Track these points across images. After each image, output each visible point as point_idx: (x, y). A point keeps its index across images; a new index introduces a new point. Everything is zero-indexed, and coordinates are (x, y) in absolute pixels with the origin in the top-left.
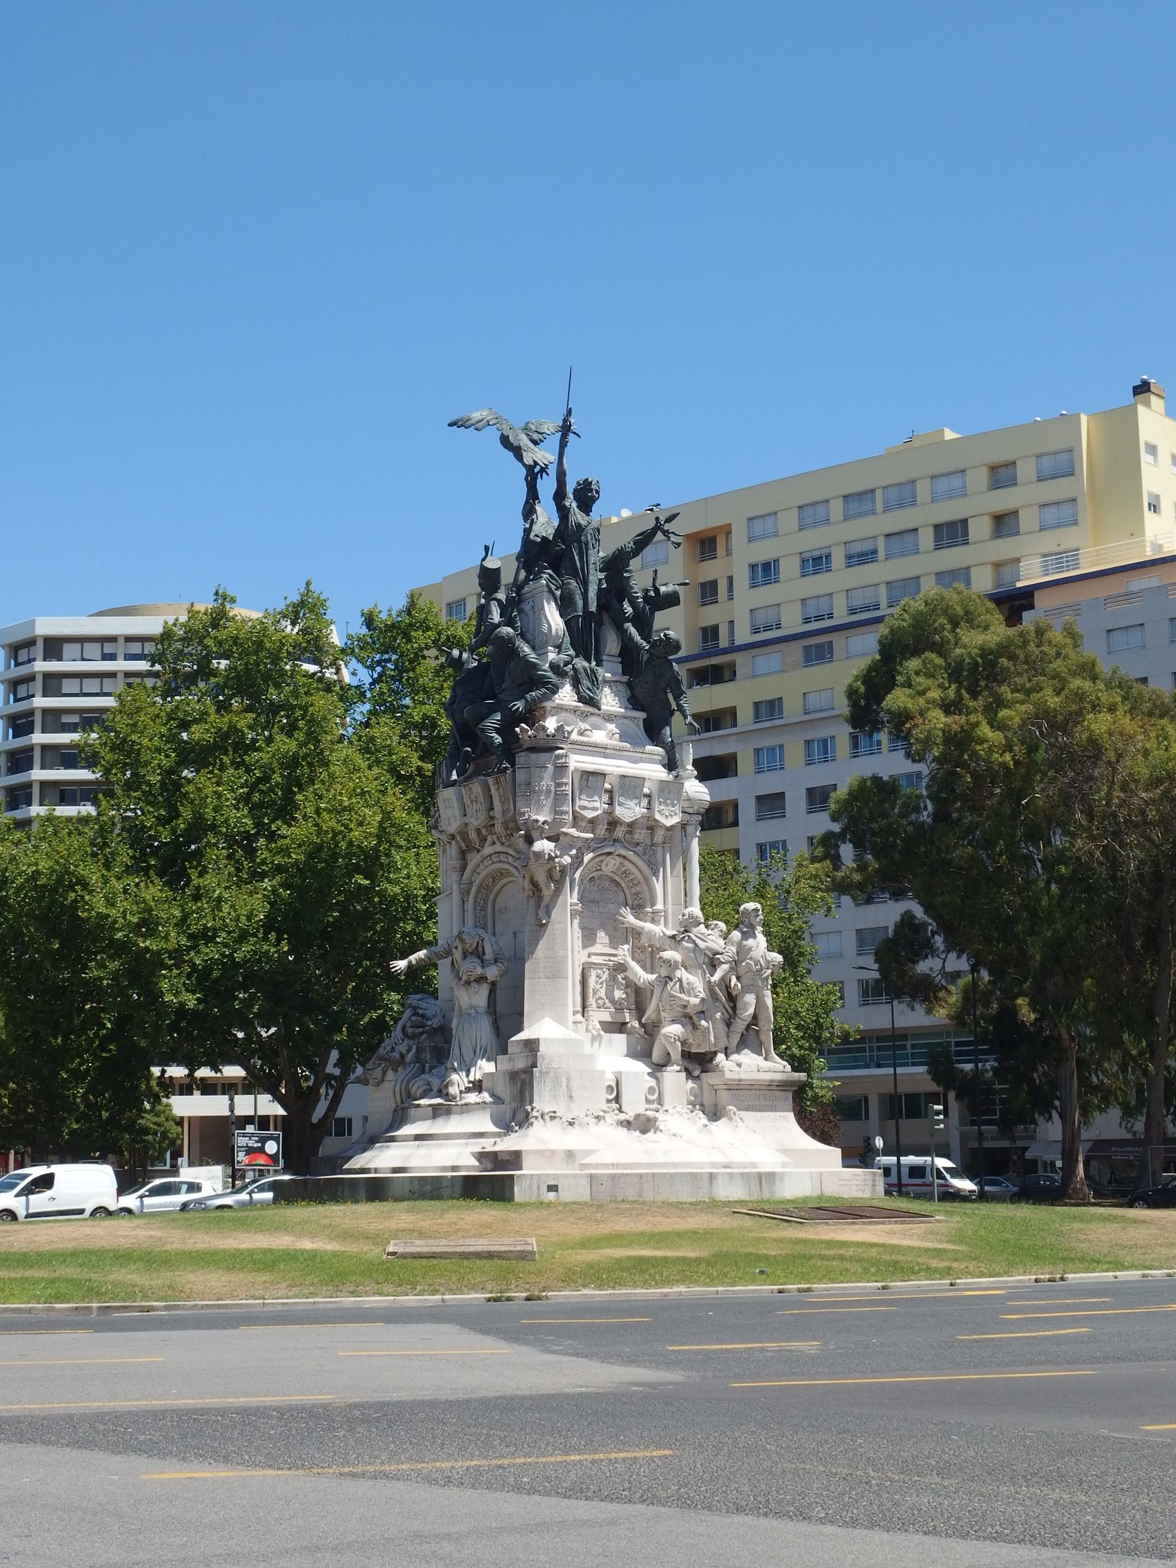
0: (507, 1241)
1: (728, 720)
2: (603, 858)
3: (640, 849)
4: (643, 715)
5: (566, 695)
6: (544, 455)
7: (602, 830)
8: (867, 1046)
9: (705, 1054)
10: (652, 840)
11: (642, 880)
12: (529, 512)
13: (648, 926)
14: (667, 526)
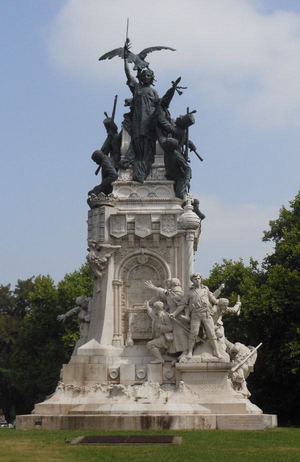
11: (162, 265)
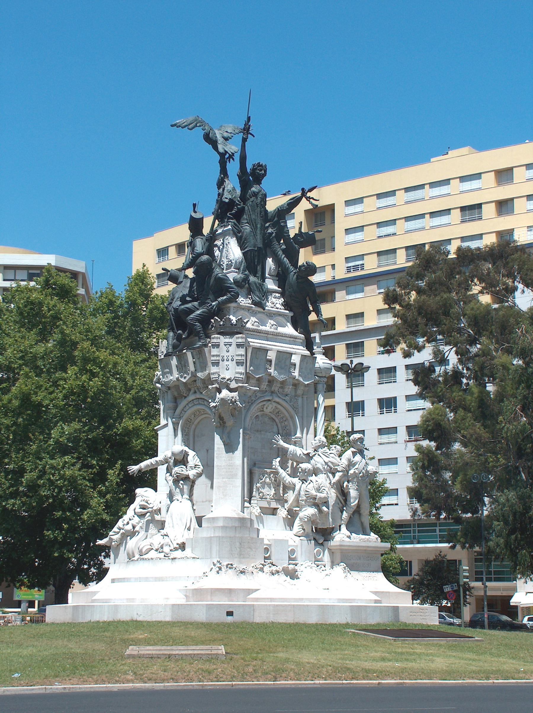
0: (435, 642)
1: (330, 326)
2: (264, 403)
3: (287, 398)
4: (291, 314)
5: (244, 301)
6: (233, 147)
7: (264, 386)
8: (412, 529)
9: (326, 529)
10: (296, 392)
11: (289, 418)
12: (220, 183)
13: (291, 448)
14: (309, 194)
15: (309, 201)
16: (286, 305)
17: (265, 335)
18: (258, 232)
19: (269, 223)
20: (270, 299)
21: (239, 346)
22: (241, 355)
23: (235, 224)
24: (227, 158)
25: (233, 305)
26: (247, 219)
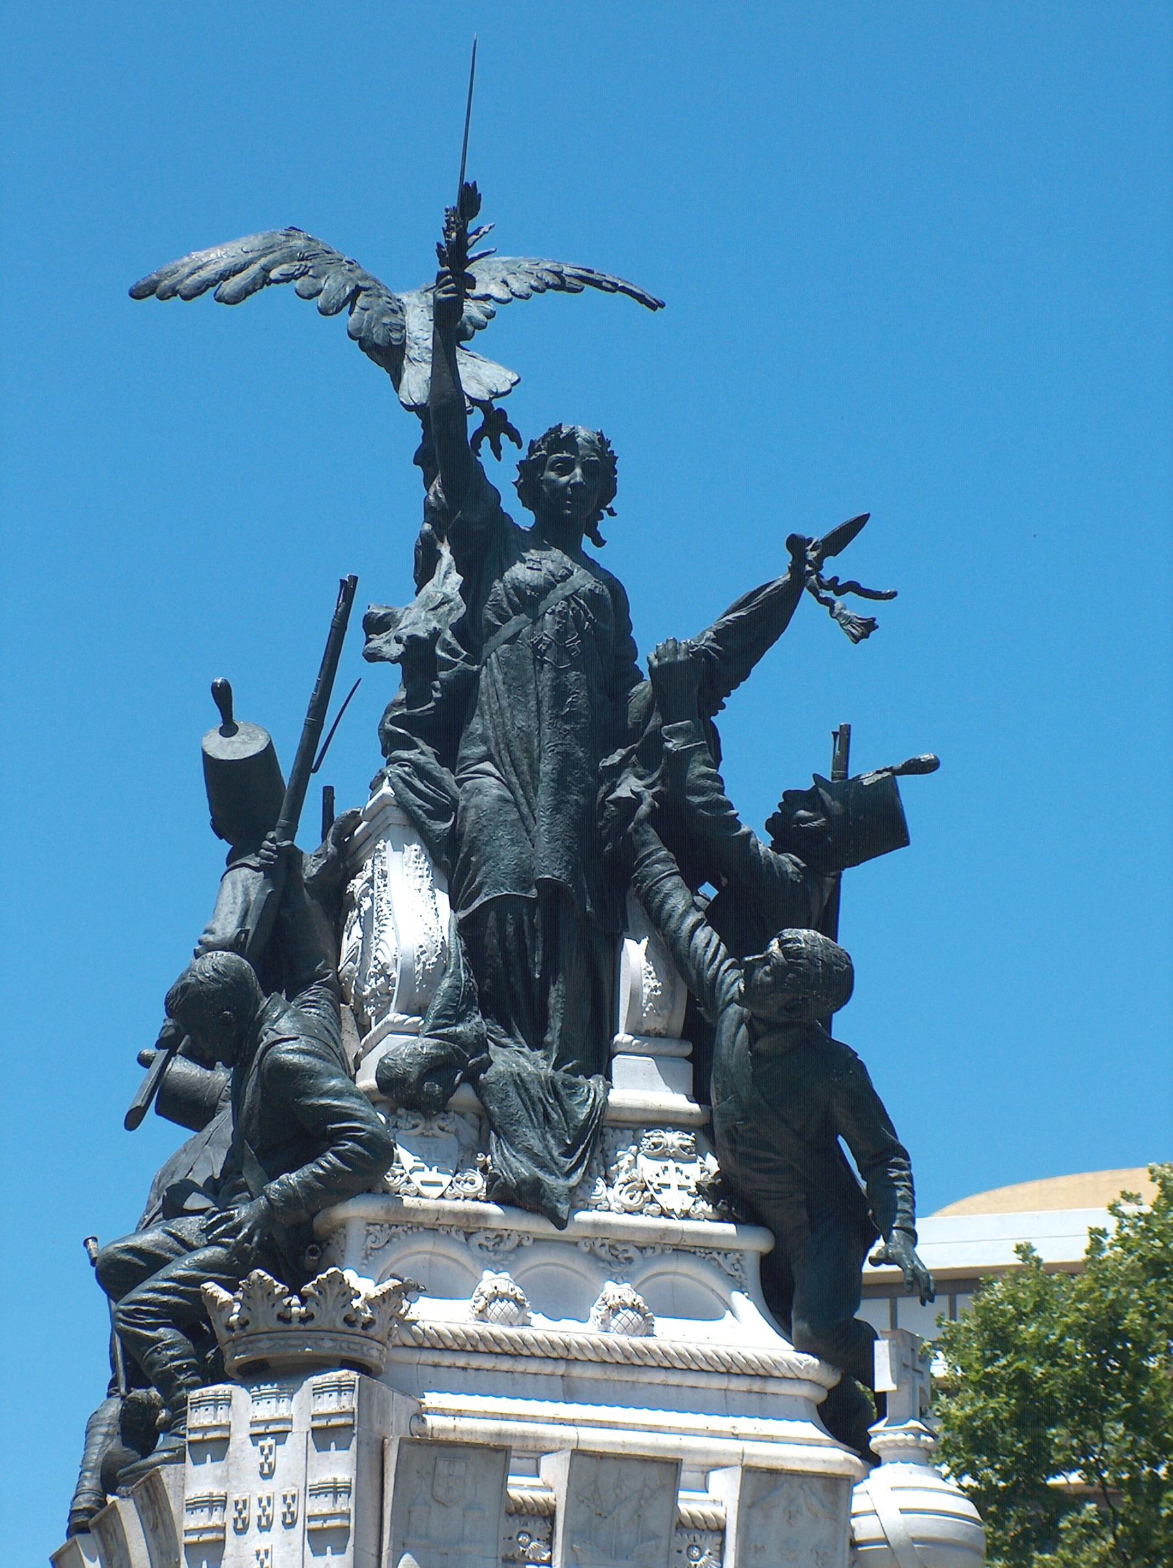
4: (757, 1243)
15: (828, 602)
16: (724, 1196)
17: (548, 1368)
18: (544, 799)
19: (623, 752)
20: (624, 1163)
21: (325, 1436)
22: (335, 1490)
23: (421, 771)
24: (478, 435)
25: (356, 1212)
26: (484, 739)
